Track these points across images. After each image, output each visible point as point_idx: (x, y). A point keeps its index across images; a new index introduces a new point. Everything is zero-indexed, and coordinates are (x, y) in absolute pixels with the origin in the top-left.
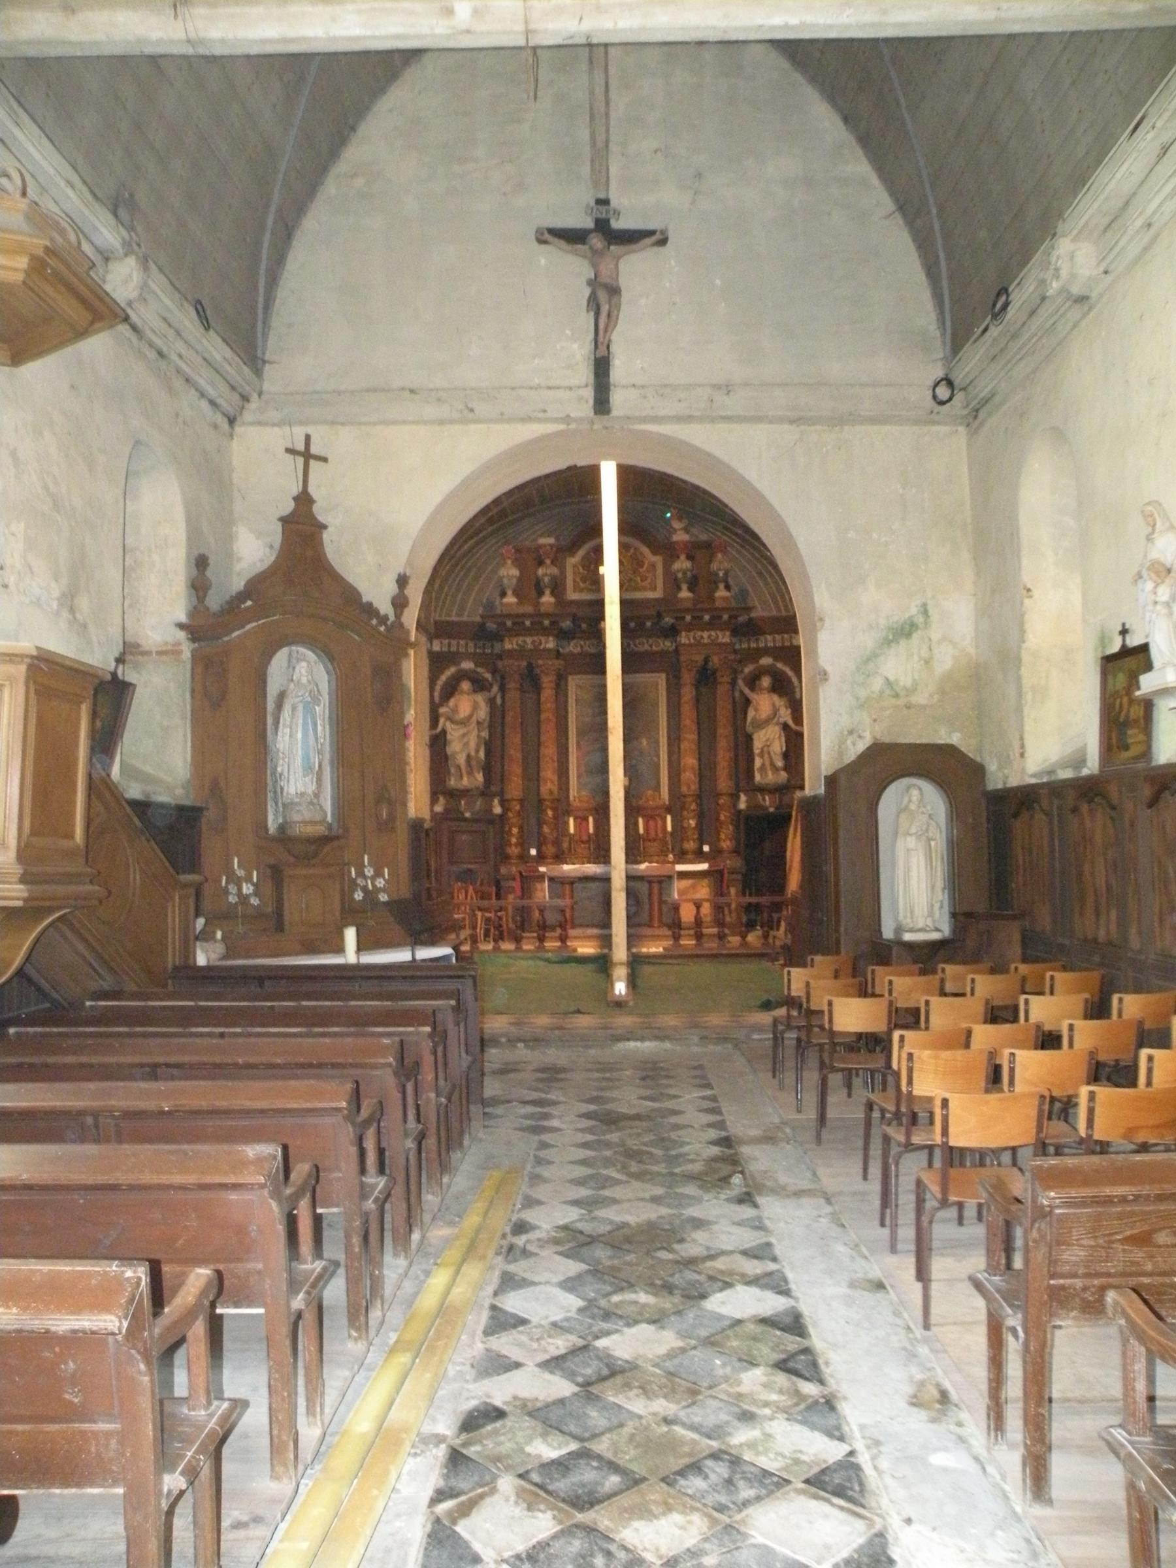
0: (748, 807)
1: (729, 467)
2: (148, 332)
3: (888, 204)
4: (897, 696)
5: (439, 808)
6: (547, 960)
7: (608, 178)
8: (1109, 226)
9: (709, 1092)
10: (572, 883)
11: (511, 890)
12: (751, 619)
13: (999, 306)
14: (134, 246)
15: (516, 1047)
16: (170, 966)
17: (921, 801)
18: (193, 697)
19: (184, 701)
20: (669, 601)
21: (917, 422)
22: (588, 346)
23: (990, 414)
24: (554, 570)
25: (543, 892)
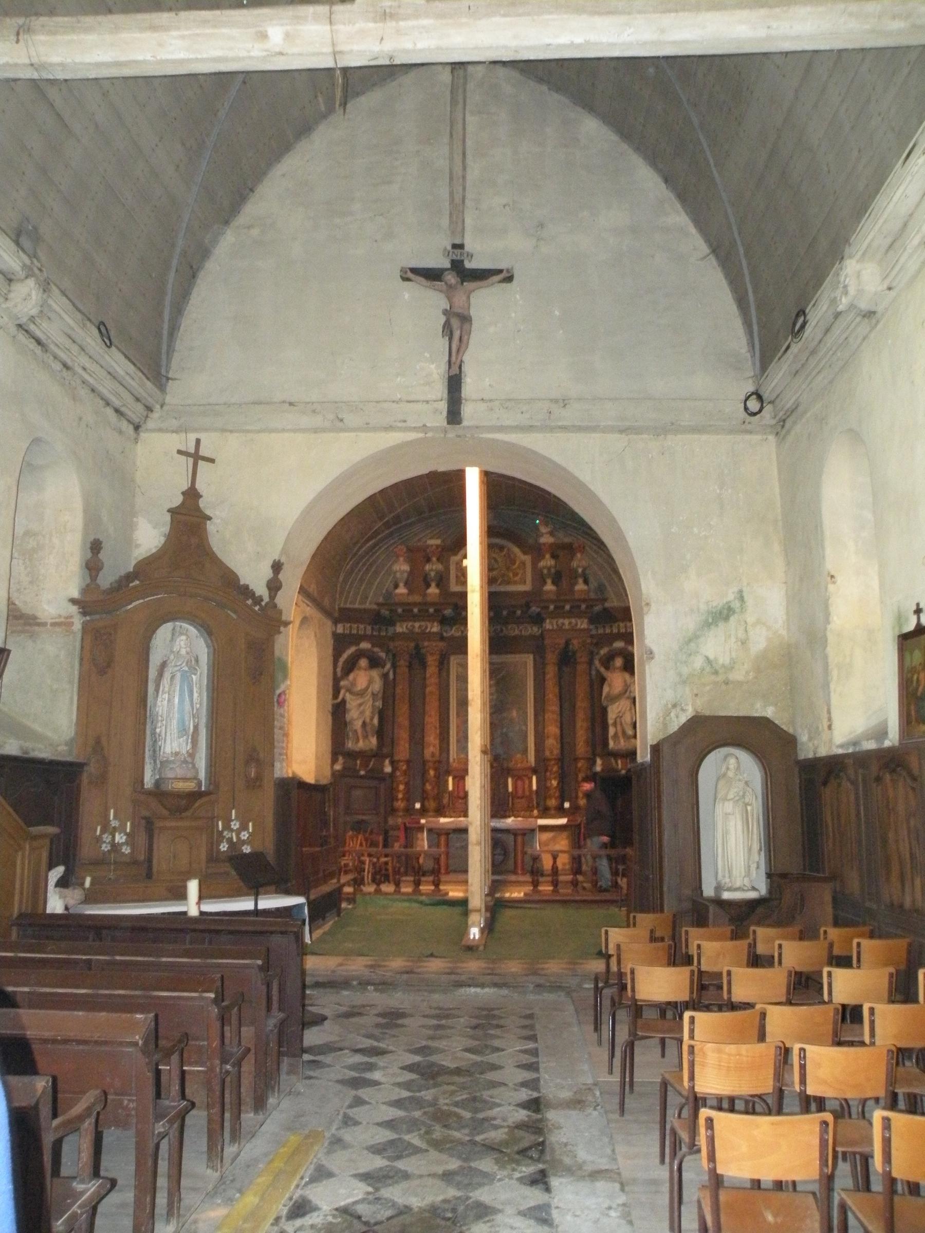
0: (603, 770)
1: (564, 469)
2: (52, 347)
3: (704, 249)
4: (716, 673)
5: (338, 767)
6: (421, 903)
7: (463, 228)
8: (890, 246)
9: (531, 1045)
10: (447, 834)
11: (397, 839)
12: (605, 609)
13: (797, 328)
14: (37, 271)
15: (366, 989)
16: (16, 912)
17: (738, 768)
18: (81, 664)
19: (72, 667)
20: (536, 594)
21: (731, 432)
22: (444, 366)
23: (795, 423)
24: (440, 567)
25: (423, 842)
